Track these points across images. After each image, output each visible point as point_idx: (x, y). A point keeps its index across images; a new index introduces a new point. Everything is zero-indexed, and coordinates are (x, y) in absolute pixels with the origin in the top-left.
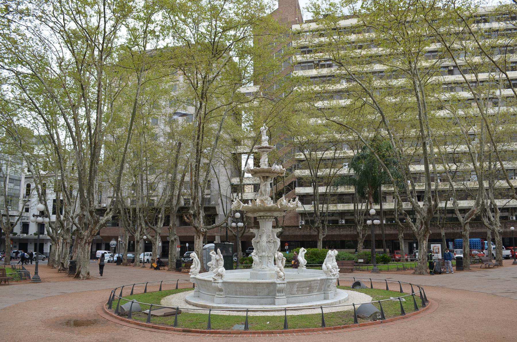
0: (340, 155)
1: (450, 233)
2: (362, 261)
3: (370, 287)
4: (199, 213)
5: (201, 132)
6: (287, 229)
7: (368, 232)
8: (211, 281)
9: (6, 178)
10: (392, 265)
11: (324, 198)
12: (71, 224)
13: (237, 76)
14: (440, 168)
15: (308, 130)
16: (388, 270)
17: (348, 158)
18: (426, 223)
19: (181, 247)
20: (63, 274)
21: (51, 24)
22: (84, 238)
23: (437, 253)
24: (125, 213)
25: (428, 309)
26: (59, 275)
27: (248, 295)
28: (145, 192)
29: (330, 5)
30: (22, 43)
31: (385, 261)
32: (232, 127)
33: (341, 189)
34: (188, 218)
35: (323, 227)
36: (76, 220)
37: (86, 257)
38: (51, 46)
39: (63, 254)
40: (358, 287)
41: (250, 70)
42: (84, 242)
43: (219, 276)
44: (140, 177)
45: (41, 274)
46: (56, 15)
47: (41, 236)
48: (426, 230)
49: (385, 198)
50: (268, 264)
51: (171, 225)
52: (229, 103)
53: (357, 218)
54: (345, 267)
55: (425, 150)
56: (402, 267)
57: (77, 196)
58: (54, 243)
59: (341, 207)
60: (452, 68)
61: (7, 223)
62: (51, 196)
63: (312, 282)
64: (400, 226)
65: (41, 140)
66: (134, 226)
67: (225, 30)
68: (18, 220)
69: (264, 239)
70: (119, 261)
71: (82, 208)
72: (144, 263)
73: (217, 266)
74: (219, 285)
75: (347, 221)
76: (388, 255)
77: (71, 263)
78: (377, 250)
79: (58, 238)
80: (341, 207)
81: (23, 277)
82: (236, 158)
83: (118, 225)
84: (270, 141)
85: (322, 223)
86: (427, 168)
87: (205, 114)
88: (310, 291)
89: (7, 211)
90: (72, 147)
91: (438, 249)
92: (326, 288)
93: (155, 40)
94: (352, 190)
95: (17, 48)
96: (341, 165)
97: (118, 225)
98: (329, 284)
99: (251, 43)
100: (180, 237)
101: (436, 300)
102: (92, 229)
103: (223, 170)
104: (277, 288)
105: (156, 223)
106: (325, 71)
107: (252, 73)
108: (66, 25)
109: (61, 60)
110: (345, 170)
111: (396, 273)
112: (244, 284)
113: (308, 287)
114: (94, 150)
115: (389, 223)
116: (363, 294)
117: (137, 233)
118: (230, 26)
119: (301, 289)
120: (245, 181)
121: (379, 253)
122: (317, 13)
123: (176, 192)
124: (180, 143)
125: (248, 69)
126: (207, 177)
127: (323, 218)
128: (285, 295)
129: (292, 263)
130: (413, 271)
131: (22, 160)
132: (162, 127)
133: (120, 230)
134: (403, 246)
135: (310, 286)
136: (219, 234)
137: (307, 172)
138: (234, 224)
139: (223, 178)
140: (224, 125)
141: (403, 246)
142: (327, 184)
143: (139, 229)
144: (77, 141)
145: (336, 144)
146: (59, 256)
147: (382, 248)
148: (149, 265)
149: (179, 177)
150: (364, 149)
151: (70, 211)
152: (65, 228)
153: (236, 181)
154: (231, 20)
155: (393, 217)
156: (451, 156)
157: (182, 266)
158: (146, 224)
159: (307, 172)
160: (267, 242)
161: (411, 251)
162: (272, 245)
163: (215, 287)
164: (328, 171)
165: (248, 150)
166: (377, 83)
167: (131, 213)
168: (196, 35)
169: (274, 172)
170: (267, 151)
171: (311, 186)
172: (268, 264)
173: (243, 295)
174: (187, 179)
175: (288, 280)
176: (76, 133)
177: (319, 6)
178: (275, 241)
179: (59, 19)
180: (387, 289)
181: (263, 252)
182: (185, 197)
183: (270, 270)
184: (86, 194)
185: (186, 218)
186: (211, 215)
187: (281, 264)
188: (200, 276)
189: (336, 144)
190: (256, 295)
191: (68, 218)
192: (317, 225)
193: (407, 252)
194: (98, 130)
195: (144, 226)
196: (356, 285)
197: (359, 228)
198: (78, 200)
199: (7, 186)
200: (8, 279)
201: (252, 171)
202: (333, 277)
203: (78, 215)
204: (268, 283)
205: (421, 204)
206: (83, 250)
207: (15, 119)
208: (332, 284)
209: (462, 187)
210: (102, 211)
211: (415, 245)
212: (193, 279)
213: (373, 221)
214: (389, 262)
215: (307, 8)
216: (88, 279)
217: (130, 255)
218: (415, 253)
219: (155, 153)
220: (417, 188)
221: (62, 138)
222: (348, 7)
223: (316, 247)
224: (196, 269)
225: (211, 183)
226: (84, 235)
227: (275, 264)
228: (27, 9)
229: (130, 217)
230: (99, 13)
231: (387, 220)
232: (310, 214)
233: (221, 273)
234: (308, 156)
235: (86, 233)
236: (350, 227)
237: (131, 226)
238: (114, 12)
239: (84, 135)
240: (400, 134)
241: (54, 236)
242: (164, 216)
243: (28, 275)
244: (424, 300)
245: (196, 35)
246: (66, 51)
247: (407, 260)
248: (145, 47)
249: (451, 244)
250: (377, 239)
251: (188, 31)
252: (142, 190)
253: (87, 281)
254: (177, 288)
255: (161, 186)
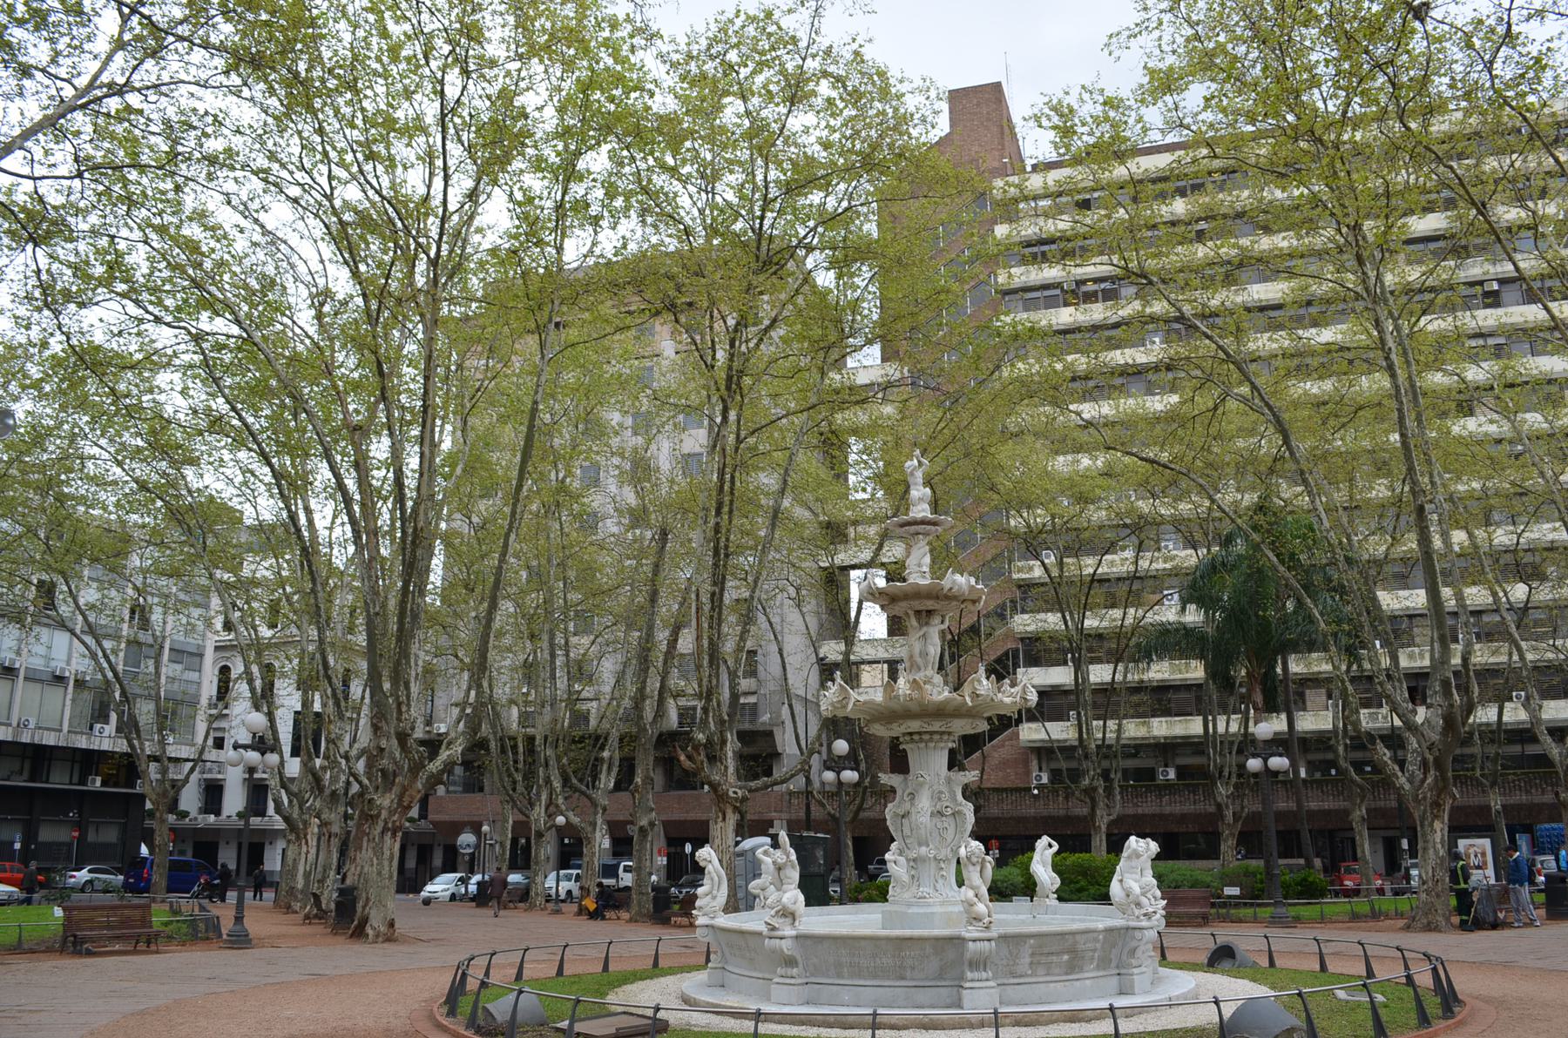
0: (1154, 566)
1: (1519, 807)
2: (1235, 891)
3: (1266, 963)
4: (724, 742)
5: (725, 499)
6: (994, 797)
7: (1253, 805)
8: (760, 934)
9: (162, 647)
10: (1335, 906)
11: (1108, 700)
12: (343, 778)
13: (829, 332)
14: (1476, 595)
15: (1053, 487)
16: (1322, 920)
17: (1175, 573)
18: (1438, 764)
19: (669, 856)
20: (319, 929)
21: (294, 191)
22: (379, 814)
23: (1479, 867)
24: (503, 751)
25: (1461, 1023)
26: (307, 929)
27: (875, 977)
28: (562, 683)
29: (1105, 103)
30: (213, 250)
31: (1310, 891)
32: (820, 484)
33: (1160, 671)
34: (689, 757)
35: (1109, 791)
36: (360, 766)
37: (385, 872)
38: (295, 259)
39: (319, 869)
40: (1227, 964)
41: (871, 310)
42: (379, 828)
43: (784, 915)
44: (545, 637)
45: (253, 924)
46: (308, 165)
47: (255, 821)
48: (1441, 788)
49: (1302, 695)
50: (937, 882)
51: (638, 780)
52: (805, 405)
53: (1214, 759)
54: (1181, 910)
55: (1425, 540)
56: (1366, 909)
57: (363, 698)
58: (293, 837)
59: (1161, 728)
60: (1495, 286)
61: (161, 782)
62: (289, 699)
63: (1078, 937)
64: (1353, 781)
65: (267, 538)
66: (529, 788)
67: (792, 189)
68: (192, 770)
69: (924, 803)
70: (482, 898)
71: (376, 728)
72: (558, 900)
73: (780, 884)
74: (786, 946)
75: (1182, 772)
76: (1317, 873)
77: (342, 892)
78: (1281, 862)
79: (305, 823)
80: (1161, 728)
81: (202, 933)
82: (834, 580)
83: (481, 789)
84: (935, 505)
85: (1105, 775)
86: (1434, 595)
87: (739, 440)
88: (1073, 967)
89: (162, 743)
90: (351, 549)
91: (1483, 854)
92: (1124, 957)
93: (590, 229)
94: (1195, 671)
95: (199, 265)
96: (1158, 597)
97: (481, 789)
98: (1134, 944)
99: (871, 228)
100: (666, 824)
101: (1488, 1000)
102: (404, 789)
103: (793, 616)
104: (968, 956)
105: (595, 777)
106: (1097, 312)
107: (875, 317)
108: (336, 193)
109: (322, 296)
110: (1169, 613)
111: (1349, 928)
112: (863, 943)
113: (1065, 954)
114: (413, 551)
115: (1318, 775)
116: (1246, 982)
117: (537, 808)
118: (806, 177)
119: (1043, 959)
120: (860, 652)
121: (1290, 868)
122: (1066, 132)
123: (654, 684)
124: (664, 534)
125: (865, 305)
126: (742, 638)
127: (1106, 764)
128: (994, 978)
129: (1011, 886)
130: (1401, 923)
131: (206, 592)
132: (613, 489)
133: (487, 804)
134: (1367, 846)
135: (1073, 951)
136: (785, 816)
137: (1053, 620)
138: (829, 776)
139: (795, 643)
140: (794, 478)
141: (1367, 846)
142: (1116, 657)
143: (544, 797)
144: (365, 531)
145: (1141, 531)
146: (307, 875)
147: (1300, 856)
148: (575, 907)
149: (662, 636)
150: (1228, 541)
151: (339, 737)
152: (327, 792)
153: (833, 650)
154: (811, 160)
155: (1330, 756)
156: (1508, 558)
157: (670, 904)
158: (566, 781)
159: (1053, 620)
160: (932, 814)
161: (1392, 865)
162: (949, 823)
163: (774, 951)
164: (1117, 613)
165: (866, 555)
166: (1263, 342)
167: (521, 749)
168: (707, 212)
169: (950, 597)
170: (926, 534)
171: (1065, 663)
172: (937, 882)
173: (860, 977)
174: (686, 643)
175: (1002, 931)
176: (363, 505)
177: (1071, 111)
178: (959, 812)
179: (316, 175)
180: (1323, 968)
181: (920, 845)
182: (682, 702)
183: (943, 903)
184: (387, 686)
185: (682, 758)
186: (759, 755)
187: (979, 879)
188: (724, 921)
189: (1141, 531)
190: (903, 978)
191: (335, 761)
192: (1087, 782)
193: (1381, 867)
194: (424, 491)
195: (557, 784)
196: (1222, 957)
197: (1223, 791)
198: (365, 711)
199: (164, 670)
200: (157, 935)
201: (881, 592)
202: (1144, 923)
203: (363, 752)
204: (937, 939)
205: (1421, 714)
206: (378, 852)
207: (189, 472)
208: (1142, 948)
209: (1550, 655)
210: (433, 745)
211: (1405, 844)
212: (705, 931)
213: (1265, 761)
214: (1323, 895)
215: (1037, 118)
216: (389, 939)
217: (514, 878)
218: (1407, 870)
219: (589, 571)
220: (1404, 662)
221: (321, 523)
222: (1160, 104)
223: (1088, 850)
224: (714, 898)
225: (759, 658)
226: (380, 808)
227: (960, 883)
228: (229, 151)
229: (516, 762)
230: (429, 157)
231: (1311, 766)
232: (1066, 750)
233: (792, 907)
234: (1055, 573)
235: (385, 801)
236: (1193, 789)
237: (520, 788)
238: (470, 149)
239: (385, 517)
240: (1340, 496)
241: (295, 816)
242: (617, 755)
243: (214, 926)
244: (1449, 999)
245: (707, 212)
246: (337, 274)
247: (1381, 891)
248: (560, 249)
249: (1523, 841)
250: (1281, 828)
251: (684, 201)
252: (553, 676)
253: (386, 945)
254: (656, 964)
255: (608, 669)
